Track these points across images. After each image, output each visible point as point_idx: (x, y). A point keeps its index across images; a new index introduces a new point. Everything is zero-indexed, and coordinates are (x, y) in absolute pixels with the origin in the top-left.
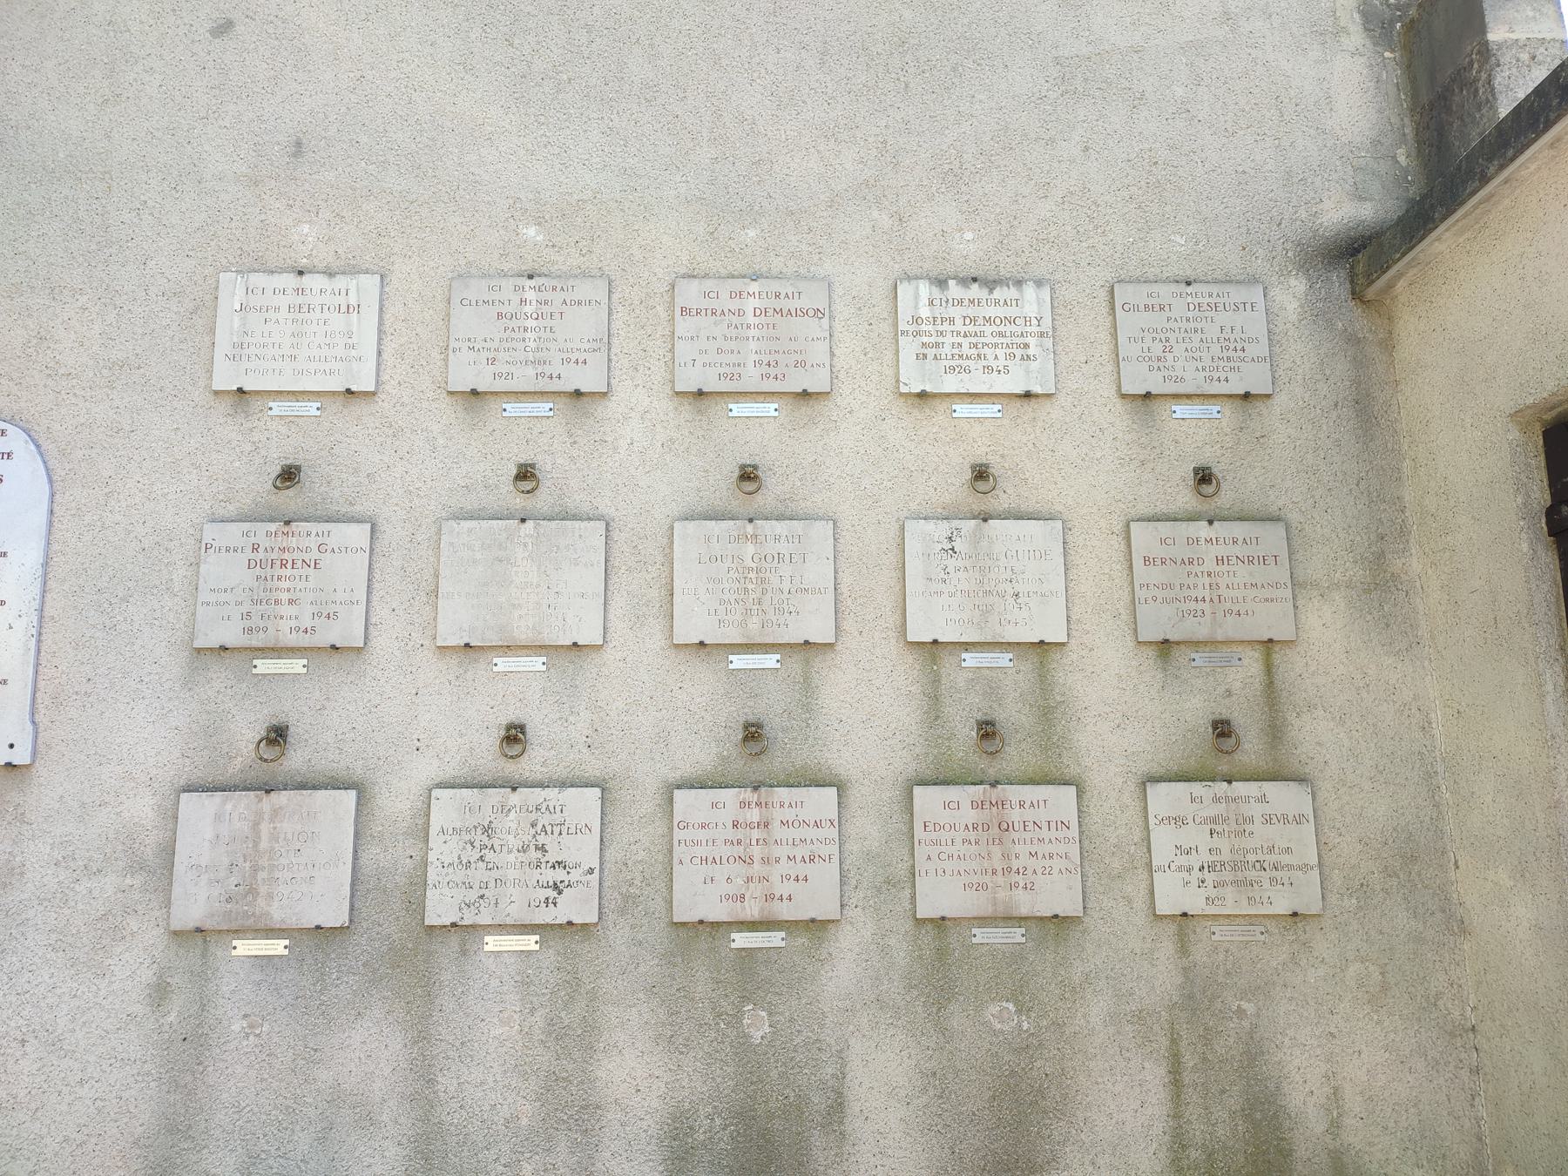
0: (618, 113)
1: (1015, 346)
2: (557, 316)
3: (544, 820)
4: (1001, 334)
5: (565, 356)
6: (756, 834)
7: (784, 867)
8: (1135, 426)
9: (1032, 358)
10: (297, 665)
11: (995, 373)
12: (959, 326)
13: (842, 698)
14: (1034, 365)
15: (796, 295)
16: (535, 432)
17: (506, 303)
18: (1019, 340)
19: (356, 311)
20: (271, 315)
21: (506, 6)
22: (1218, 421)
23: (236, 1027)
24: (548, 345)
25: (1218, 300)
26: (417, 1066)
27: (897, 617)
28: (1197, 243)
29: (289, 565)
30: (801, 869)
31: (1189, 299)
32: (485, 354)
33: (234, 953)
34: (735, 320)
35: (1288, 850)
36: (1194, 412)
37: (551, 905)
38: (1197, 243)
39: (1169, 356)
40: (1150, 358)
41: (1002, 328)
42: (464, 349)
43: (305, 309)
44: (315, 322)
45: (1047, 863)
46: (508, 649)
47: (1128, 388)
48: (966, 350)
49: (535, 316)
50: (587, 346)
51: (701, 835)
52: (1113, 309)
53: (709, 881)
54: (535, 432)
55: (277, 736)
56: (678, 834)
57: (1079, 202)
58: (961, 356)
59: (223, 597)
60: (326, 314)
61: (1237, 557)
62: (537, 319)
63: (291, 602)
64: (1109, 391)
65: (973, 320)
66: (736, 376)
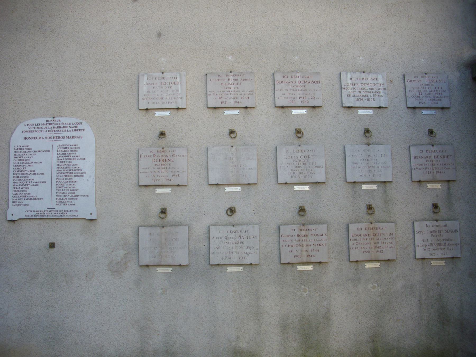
0: (255, 21)
1: (376, 92)
3: (243, 234)
4: (372, 89)
5: (242, 96)
6: (304, 238)
7: (312, 247)
8: (411, 117)
9: (381, 96)
10: (168, 190)
11: (371, 101)
12: (360, 86)
13: (328, 198)
14: (382, 99)
15: (311, 77)
18: (377, 91)
19: (179, 84)
20: (155, 85)
22: (435, 115)
23: (159, 292)
25: (434, 79)
26: (210, 302)
27: (344, 174)
28: (428, 61)
29: (164, 161)
30: (317, 248)
31: (426, 79)
33: (157, 272)
34: (293, 84)
35: (452, 240)
36: (428, 112)
37: (246, 259)
38: (428, 61)
39: (421, 96)
40: (415, 96)
41: (372, 87)
43: (164, 83)
44: (168, 87)
45: (386, 245)
46: (229, 185)
47: (410, 105)
48: (362, 94)
49: (233, 84)
50: (249, 93)
51: (288, 238)
52: (404, 81)
53: (291, 252)
55: (164, 211)
56: (282, 239)
57: (394, 48)
58: (360, 96)
61: (440, 156)
62: (233, 85)
63: (166, 172)
64: (404, 106)
65: (364, 85)
66: (294, 102)
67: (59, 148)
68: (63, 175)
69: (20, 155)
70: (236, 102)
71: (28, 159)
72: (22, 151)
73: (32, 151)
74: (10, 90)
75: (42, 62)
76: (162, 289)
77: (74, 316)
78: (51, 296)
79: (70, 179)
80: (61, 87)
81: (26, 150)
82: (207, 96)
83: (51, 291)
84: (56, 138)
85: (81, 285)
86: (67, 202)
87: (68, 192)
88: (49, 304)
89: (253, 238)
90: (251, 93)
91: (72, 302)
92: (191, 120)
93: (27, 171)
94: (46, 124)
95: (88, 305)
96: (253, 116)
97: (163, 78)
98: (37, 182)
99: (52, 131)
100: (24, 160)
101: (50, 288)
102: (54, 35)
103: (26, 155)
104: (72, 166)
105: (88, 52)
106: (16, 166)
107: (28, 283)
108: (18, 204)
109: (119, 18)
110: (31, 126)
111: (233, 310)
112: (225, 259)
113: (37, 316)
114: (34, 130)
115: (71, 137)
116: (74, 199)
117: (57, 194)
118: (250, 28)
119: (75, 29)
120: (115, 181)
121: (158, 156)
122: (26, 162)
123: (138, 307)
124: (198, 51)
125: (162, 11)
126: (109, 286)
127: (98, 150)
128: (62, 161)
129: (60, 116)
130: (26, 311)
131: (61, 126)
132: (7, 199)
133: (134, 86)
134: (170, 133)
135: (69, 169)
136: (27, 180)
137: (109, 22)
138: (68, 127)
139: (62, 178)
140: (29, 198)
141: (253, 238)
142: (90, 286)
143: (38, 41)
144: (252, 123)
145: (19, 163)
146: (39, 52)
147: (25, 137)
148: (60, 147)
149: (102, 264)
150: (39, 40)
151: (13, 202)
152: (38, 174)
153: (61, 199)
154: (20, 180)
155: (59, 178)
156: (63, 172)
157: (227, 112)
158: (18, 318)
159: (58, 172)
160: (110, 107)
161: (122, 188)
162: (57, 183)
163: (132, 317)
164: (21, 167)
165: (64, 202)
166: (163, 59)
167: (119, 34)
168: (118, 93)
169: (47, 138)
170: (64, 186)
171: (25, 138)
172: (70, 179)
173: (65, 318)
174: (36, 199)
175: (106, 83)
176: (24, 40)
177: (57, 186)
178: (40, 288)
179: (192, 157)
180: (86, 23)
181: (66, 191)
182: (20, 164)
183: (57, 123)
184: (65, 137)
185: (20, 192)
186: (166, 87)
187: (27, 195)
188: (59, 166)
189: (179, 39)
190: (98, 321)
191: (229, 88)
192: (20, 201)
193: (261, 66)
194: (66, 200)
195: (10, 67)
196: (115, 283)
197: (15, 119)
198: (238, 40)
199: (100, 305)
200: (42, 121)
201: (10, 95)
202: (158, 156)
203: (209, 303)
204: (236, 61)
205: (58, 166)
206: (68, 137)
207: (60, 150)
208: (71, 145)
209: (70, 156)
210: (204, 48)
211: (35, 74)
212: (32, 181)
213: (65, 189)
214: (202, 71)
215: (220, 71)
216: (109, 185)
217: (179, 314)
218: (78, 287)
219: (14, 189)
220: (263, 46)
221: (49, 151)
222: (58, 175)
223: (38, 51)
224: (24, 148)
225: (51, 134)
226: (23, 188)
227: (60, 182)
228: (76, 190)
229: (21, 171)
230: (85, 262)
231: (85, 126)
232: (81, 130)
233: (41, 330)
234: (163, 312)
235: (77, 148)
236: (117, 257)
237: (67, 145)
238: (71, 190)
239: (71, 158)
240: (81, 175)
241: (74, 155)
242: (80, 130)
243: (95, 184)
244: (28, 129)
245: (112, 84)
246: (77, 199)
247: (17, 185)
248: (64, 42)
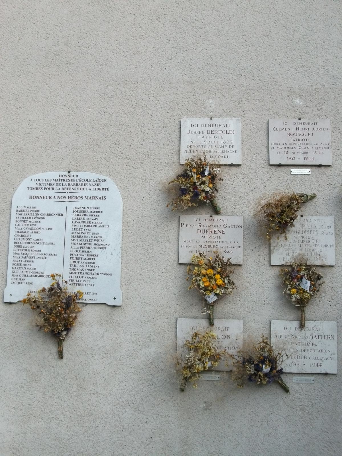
0: (329, 54)
2: (311, 134)
5: (315, 150)
16: (304, 180)
17: (291, 129)
20: (201, 135)
21: (283, 13)
24: (308, 146)
32: (284, 150)
42: (276, 148)
49: (302, 134)
50: (323, 146)
54: (304, 180)
59: (189, 244)
60: (222, 134)
67: (76, 211)
68: (79, 246)
69: (24, 218)
70: (307, 158)
71: (34, 223)
72: (27, 213)
73: (40, 214)
74: (13, 136)
75: (55, 102)
76: (205, 402)
77: (86, 434)
78: (56, 405)
79: (88, 252)
80: (79, 133)
81: (31, 212)
82: (269, 150)
83: (56, 398)
84: (71, 198)
85: (97, 392)
86: (84, 281)
87: (85, 268)
88: (53, 416)
89: (329, 338)
90: (327, 146)
91: (84, 414)
92: (247, 180)
93: (32, 240)
94: (59, 180)
95: (106, 420)
96: (329, 177)
97: (211, 125)
98: (44, 254)
99: (67, 189)
100: (29, 225)
101: (55, 394)
102: (71, 69)
103: (31, 218)
104: (91, 235)
105: (114, 90)
106: (18, 232)
107: (26, 385)
108: (19, 281)
109: (154, 48)
110: (39, 182)
111: (301, 436)
112: (291, 365)
113: (37, 431)
114: (43, 187)
115: (92, 198)
116: (92, 278)
117: (71, 271)
118: (323, 62)
119: (97, 61)
120: (147, 256)
121: (205, 226)
122: (31, 227)
123: (172, 425)
124: (256, 91)
125: (209, 41)
126: (134, 395)
127: (126, 216)
128: (78, 228)
129: (77, 170)
130: (21, 423)
131: (79, 183)
132: (5, 274)
133: (173, 134)
134: (220, 197)
135: (87, 239)
136: (32, 251)
137: (142, 53)
138: (88, 185)
139: (77, 249)
140: (33, 274)
141: (329, 338)
142: (109, 394)
143: (51, 75)
144: (328, 185)
145: (23, 229)
146: (52, 89)
147: (31, 195)
148: (77, 210)
149: (127, 365)
150: (52, 74)
151: (12, 279)
152: (46, 244)
153: (76, 277)
154: (23, 250)
155: (74, 250)
156: (79, 242)
157: (295, 171)
158: (10, 432)
159: (72, 242)
160: (143, 161)
161: (156, 265)
162: (72, 256)
163: (164, 438)
164: (25, 234)
165: (80, 281)
166: (211, 101)
167: (154, 68)
168: (153, 143)
169: (59, 198)
170: (80, 261)
171: (31, 197)
172: (88, 252)
173: (73, 435)
174: (42, 276)
175: (137, 130)
176: (33, 74)
177: (71, 260)
178: (42, 394)
179: (249, 228)
180: (112, 53)
181: (83, 268)
182: (23, 230)
183: (73, 178)
184: (84, 198)
185: (22, 266)
186: (215, 137)
187: (31, 271)
188: (75, 235)
189: (232, 76)
190: (118, 442)
191: (297, 140)
192: (22, 278)
193: (338, 112)
194: (82, 279)
195: (15, 106)
196: (143, 391)
197: (19, 172)
198: (308, 77)
199: (121, 420)
200: (54, 175)
201: (14, 142)
202: (205, 226)
203: (268, 425)
204: (306, 106)
205: (73, 235)
206: (87, 198)
207: (77, 214)
208: (90, 208)
209: (89, 222)
210: (264, 88)
211: (46, 116)
212: (39, 253)
213: (82, 264)
214: (261, 117)
215: (286, 117)
216: (139, 261)
217: (227, 438)
218: (93, 395)
219: (14, 262)
220: (340, 86)
221: (62, 215)
222: (72, 246)
223: (50, 87)
224: (30, 209)
225: (65, 193)
226: (26, 261)
227: (75, 255)
228: (96, 267)
229: (25, 239)
230: (104, 361)
231: (110, 183)
232: (104, 189)
233: (40, 450)
234: (206, 434)
235: (99, 212)
236: (147, 356)
237: (85, 208)
238: (89, 266)
239: (91, 224)
240: (103, 246)
241: (95, 221)
242: (103, 189)
243: (120, 259)
244: (35, 186)
245: (145, 131)
246: (96, 278)
247: (19, 257)
248: (84, 76)
